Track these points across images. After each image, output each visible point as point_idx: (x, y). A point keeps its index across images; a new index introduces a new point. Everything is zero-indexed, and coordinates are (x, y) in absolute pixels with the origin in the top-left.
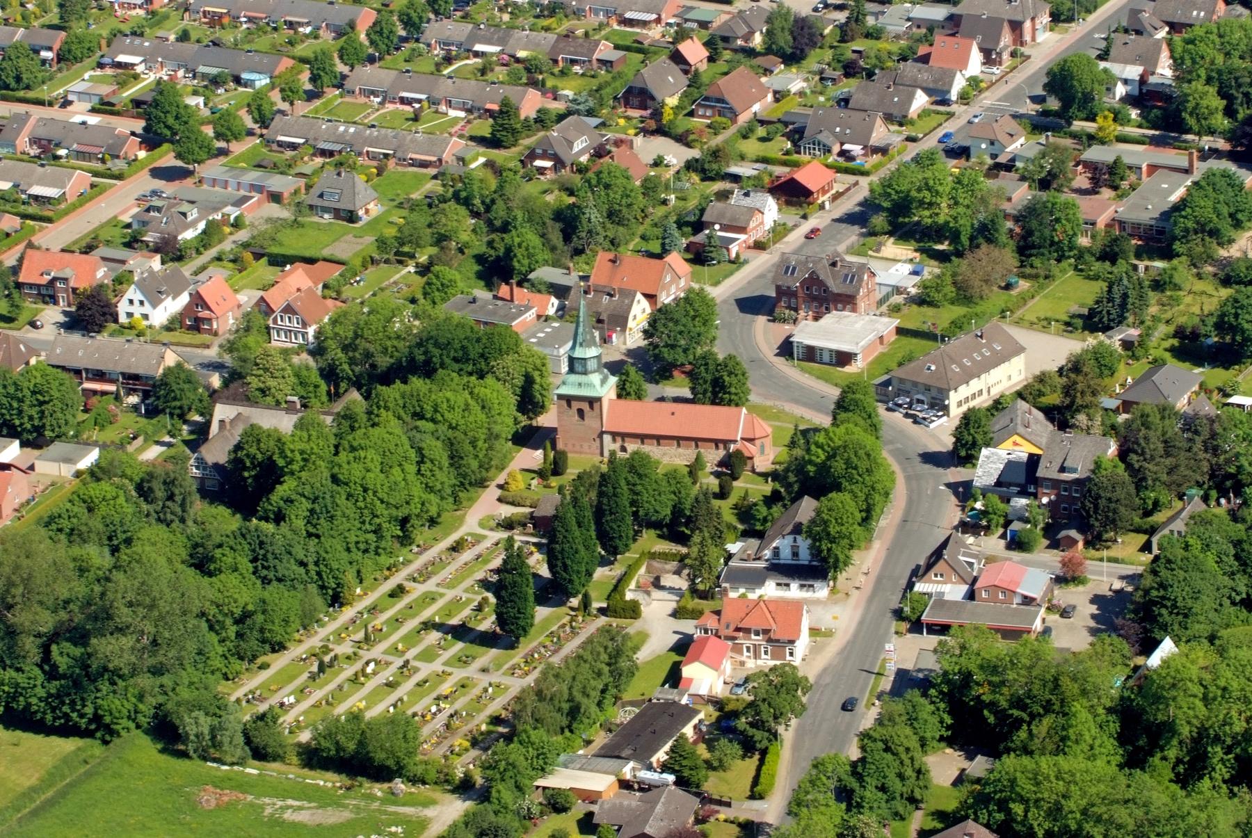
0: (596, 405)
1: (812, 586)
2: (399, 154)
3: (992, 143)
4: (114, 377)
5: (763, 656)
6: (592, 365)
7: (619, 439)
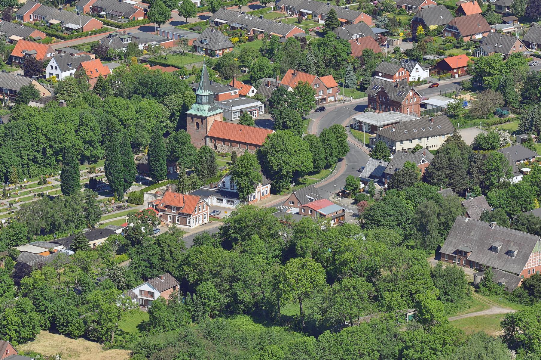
1: (233, 202)
2: (267, 32)
4: (6, 91)
5: (177, 222)
6: (206, 99)
7: (213, 141)
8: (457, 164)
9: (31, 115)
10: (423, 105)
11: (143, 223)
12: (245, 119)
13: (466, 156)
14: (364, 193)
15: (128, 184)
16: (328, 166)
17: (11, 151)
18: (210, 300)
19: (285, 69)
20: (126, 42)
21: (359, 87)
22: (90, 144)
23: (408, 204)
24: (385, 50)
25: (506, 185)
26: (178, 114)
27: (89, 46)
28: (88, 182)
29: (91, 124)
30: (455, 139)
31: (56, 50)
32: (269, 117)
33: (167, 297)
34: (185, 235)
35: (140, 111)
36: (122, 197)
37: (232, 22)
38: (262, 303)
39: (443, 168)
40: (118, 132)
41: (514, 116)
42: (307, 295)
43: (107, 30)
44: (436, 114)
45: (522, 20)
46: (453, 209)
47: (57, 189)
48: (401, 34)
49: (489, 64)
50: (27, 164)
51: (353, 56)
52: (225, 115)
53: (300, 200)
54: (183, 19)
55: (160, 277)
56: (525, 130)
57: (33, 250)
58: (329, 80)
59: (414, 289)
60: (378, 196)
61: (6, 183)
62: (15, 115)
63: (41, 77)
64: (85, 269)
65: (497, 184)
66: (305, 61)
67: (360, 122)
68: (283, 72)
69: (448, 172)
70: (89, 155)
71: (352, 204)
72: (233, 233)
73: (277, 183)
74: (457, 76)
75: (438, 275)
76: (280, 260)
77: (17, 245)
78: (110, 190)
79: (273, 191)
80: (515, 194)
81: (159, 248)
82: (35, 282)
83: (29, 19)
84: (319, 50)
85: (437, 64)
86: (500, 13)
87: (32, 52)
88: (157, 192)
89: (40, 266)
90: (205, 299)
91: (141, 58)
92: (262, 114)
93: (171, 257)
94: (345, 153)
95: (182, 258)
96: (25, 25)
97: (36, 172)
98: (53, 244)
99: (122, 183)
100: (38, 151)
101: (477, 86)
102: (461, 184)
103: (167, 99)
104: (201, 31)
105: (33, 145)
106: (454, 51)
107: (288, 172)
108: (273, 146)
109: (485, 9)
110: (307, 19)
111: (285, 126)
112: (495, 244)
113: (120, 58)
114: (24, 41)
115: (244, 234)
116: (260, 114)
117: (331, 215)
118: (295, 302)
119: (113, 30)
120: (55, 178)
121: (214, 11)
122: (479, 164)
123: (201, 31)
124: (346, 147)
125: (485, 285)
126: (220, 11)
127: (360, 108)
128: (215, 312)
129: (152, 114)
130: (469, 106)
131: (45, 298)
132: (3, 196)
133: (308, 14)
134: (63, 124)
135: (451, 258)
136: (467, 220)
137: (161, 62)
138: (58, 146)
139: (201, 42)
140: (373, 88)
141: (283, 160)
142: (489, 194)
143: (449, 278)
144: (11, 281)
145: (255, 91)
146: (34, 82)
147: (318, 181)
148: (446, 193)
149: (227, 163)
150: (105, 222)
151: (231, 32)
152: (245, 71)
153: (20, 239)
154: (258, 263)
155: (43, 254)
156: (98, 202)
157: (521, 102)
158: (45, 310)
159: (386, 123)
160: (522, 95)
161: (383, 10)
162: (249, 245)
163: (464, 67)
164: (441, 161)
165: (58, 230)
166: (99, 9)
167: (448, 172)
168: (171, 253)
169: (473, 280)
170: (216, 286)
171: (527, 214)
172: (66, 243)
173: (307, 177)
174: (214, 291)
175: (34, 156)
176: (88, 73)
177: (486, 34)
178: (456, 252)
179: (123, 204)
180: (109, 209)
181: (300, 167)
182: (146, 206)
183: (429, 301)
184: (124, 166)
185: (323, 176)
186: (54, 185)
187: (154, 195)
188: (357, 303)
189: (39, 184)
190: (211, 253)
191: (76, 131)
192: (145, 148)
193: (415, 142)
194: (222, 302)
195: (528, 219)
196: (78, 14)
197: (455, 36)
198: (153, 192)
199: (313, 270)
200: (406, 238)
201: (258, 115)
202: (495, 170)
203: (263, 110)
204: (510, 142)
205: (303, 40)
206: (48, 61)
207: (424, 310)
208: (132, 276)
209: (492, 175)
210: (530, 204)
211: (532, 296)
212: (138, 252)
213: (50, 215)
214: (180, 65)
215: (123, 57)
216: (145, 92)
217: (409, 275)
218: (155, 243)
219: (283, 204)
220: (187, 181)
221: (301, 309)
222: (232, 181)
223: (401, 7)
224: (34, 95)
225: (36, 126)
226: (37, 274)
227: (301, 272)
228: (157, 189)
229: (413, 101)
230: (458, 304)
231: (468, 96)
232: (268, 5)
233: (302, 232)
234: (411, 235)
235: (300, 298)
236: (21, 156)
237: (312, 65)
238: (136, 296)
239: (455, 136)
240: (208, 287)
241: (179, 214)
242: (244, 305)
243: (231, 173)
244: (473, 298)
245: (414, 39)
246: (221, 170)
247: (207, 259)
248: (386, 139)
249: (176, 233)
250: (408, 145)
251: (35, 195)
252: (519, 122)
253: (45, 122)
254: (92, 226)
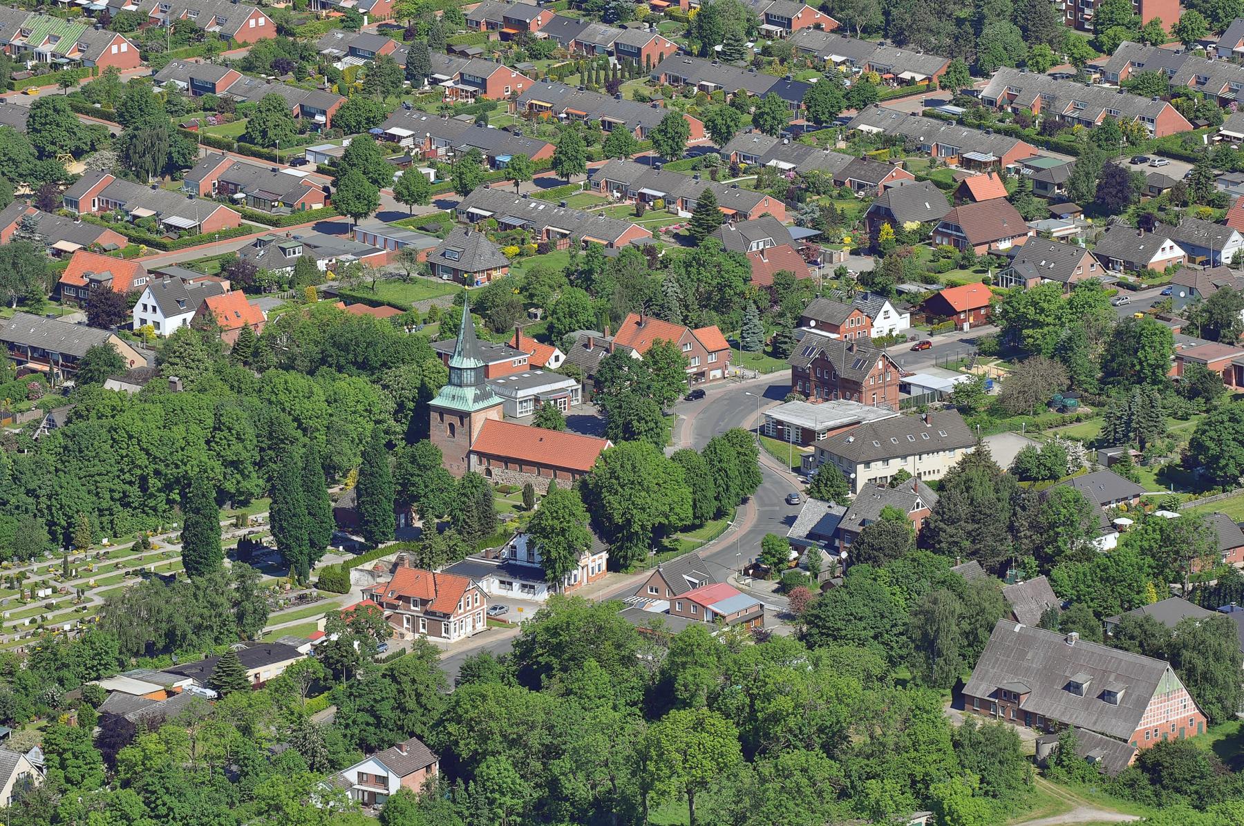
0: (466, 421)
1: (533, 587)
2: (573, 236)
3: (1191, 292)
4: (55, 357)
5: (422, 630)
6: (469, 377)
8: (988, 512)
9: (113, 409)
10: (905, 388)
11: (357, 632)
12: (546, 416)
13: (1006, 495)
14: (798, 569)
15: (318, 550)
16: (719, 514)
17: (77, 483)
18: (503, 794)
19: (620, 311)
20: (292, 256)
21: (769, 349)
22: (236, 468)
23: (894, 594)
24: (816, 273)
25: (1087, 554)
26: (411, 405)
27: (217, 264)
28: (235, 546)
29: (237, 427)
30: (981, 456)
31: (150, 272)
32: (591, 410)
33: (416, 788)
34: (443, 656)
35: (336, 401)
36: (306, 578)
37: (503, 214)
38: (611, 800)
39: (959, 520)
40: (292, 443)
41: (1088, 410)
42: (703, 784)
43: (249, 231)
44: (930, 404)
45: (1089, 211)
46: (987, 605)
47: (172, 560)
48: (848, 240)
49: (1035, 304)
50: (110, 509)
51: (754, 284)
52: (505, 407)
53: (669, 584)
54: (403, 208)
55: (400, 747)
56: (1115, 439)
57: (133, 687)
58: (712, 336)
59: (919, 770)
60: (827, 576)
61: (66, 548)
62: (81, 407)
63: (123, 327)
64: (246, 730)
65: (1068, 552)
66: (660, 297)
67: (780, 422)
68: (616, 318)
69: (970, 527)
70: (233, 491)
71: (774, 591)
72: (542, 655)
73: (620, 548)
74: (966, 326)
75: (967, 742)
76: (641, 709)
77: (98, 678)
78: (281, 562)
79: (614, 565)
80: (1108, 572)
81: (394, 687)
82: (146, 757)
83: (90, 207)
84: (688, 273)
85: (926, 301)
86: (1044, 197)
87: (103, 276)
88: (376, 567)
89: (154, 724)
90: (493, 791)
91: (323, 287)
92: (578, 406)
93: (419, 703)
94: (753, 487)
95: (442, 708)
96: (84, 220)
97: (127, 524)
98: (172, 677)
99: (306, 549)
100: (131, 483)
101: (1011, 347)
102: (995, 553)
103: (389, 376)
104: (440, 233)
105: (122, 470)
106: (957, 275)
107: (643, 527)
108: (613, 473)
109: (1014, 187)
110: (653, 209)
111: (629, 434)
112: (1078, 678)
113: (280, 287)
114: (85, 254)
115: (565, 656)
116: (573, 403)
117: (735, 616)
118: (680, 799)
119: (264, 231)
120: (165, 536)
121: (465, 191)
122: (1032, 511)
123: (440, 233)
124: (756, 474)
125: (1059, 763)
126: (477, 191)
127: (777, 393)
128: (513, 817)
129: (360, 407)
130: (996, 390)
131: (167, 789)
132: (62, 575)
133: (655, 197)
134: (182, 428)
135: (985, 704)
136: (1017, 629)
137: (365, 295)
138: (171, 472)
139: (444, 255)
140: (803, 354)
141: (633, 503)
142: (1054, 572)
143: (989, 749)
144: (96, 754)
145: (562, 357)
146: (114, 339)
147: (702, 545)
148: (969, 571)
149: (515, 506)
150: (275, 629)
151: (503, 234)
152: (536, 316)
153: (106, 666)
154: (603, 719)
155: (153, 697)
156: (262, 589)
157: (1102, 381)
158: (167, 816)
159: (831, 424)
160: (1104, 366)
161: (807, 190)
162: (577, 680)
163: (979, 308)
164: (955, 505)
165: (181, 646)
166: (231, 186)
167: (970, 527)
168: (418, 695)
169: (1033, 752)
170: (515, 765)
171: (1136, 614)
172: (200, 673)
173: (678, 535)
174: (511, 776)
175: (124, 493)
176: (221, 322)
177: (1021, 241)
178: (997, 694)
179: (307, 592)
180: (281, 602)
181: (667, 518)
182: (354, 599)
183: (958, 798)
184: (309, 513)
185: (711, 533)
186: (166, 550)
187: (371, 573)
188: (810, 803)
189: (135, 549)
190: (504, 697)
191: (208, 442)
192: (345, 476)
193: (895, 466)
194: (528, 798)
195: (1141, 626)
196: (191, 197)
197: (957, 245)
198: (368, 566)
199: (715, 734)
200: (892, 662)
201: (570, 407)
202: (1064, 524)
203: (580, 397)
204: (1087, 464)
205: (650, 251)
206: (137, 295)
207: (948, 818)
208: (340, 743)
209: (1058, 534)
210: (1138, 593)
211: (1158, 786)
212: (351, 694)
213: (164, 615)
214: (401, 302)
215: (286, 286)
216: (342, 361)
217: (909, 743)
218: (384, 676)
219: (638, 590)
220: (439, 543)
221: (692, 813)
222: (531, 544)
223: (844, 183)
224: (114, 365)
225: (127, 432)
226: (150, 741)
227: (693, 739)
228: (375, 561)
229: (884, 379)
230: (1008, 802)
231: (993, 369)
232: (572, 179)
233: (687, 655)
234: (901, 657)
235: (689, 792)
236: (97, 494)
237: (675, 304)
238: (351, 785)
239: (978, 453)
240: (500, 768)
241: (426, 613)
242: (572, 804)
243: (529, 530)
244: (1036, 789)
245: (874, 249)
246: (504, 521)
247: (496, 709)
248: (836, 458)
249: (425, 652)
250: (879, 470)
251: (127, 573)
252: (1101, 422)
253: (145, 423)
254: (250, 638)
